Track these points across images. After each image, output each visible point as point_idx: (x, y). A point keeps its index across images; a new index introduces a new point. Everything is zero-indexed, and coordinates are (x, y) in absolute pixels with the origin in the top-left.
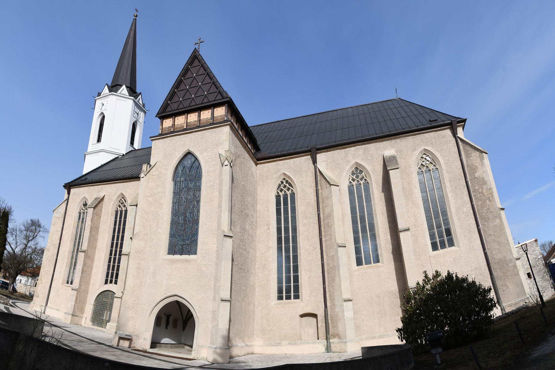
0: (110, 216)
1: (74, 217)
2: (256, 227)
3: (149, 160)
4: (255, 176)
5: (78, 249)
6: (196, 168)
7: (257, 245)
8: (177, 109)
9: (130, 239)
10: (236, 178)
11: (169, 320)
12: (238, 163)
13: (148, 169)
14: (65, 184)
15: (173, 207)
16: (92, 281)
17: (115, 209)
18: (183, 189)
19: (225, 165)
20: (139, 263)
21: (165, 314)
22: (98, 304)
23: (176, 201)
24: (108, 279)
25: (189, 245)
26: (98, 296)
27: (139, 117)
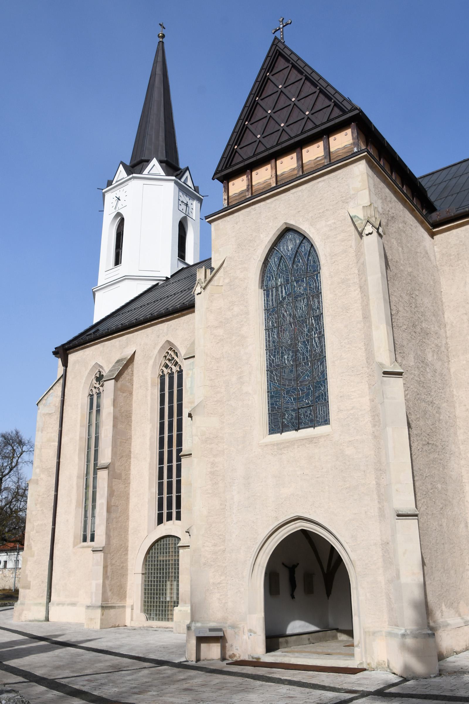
0: (150, 388)
1: (79, 406)
2: (448, 357)
3: (210, 263)
4: (432, 258)
5: (95, 465)
6: (305, 254)
7: (455, 393)
8: (254, 155)
9: (189, 417)
10: (394, 260)
11: (294, 578)
12: (393, 231)
13: (209, 276)
14: (56, 348)
15: (268, 339)
16: (132, 525)
17: (158, 372)
18: (284, 299)
19: (367, 233)
20: (212, 464)
21: (283, 564)
22: (150, 571)
23: (273, 325)
24: (163, 513)
25: (310, 406)
26: (148, 552)
27: (190, 210)
